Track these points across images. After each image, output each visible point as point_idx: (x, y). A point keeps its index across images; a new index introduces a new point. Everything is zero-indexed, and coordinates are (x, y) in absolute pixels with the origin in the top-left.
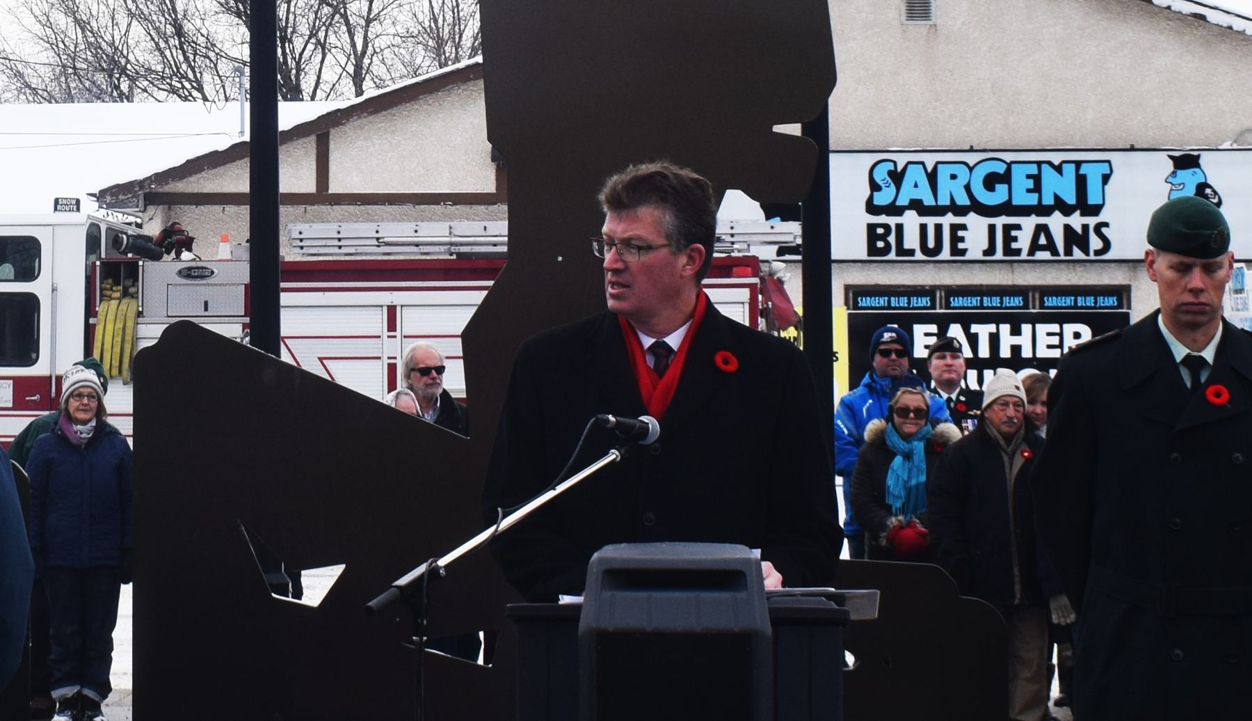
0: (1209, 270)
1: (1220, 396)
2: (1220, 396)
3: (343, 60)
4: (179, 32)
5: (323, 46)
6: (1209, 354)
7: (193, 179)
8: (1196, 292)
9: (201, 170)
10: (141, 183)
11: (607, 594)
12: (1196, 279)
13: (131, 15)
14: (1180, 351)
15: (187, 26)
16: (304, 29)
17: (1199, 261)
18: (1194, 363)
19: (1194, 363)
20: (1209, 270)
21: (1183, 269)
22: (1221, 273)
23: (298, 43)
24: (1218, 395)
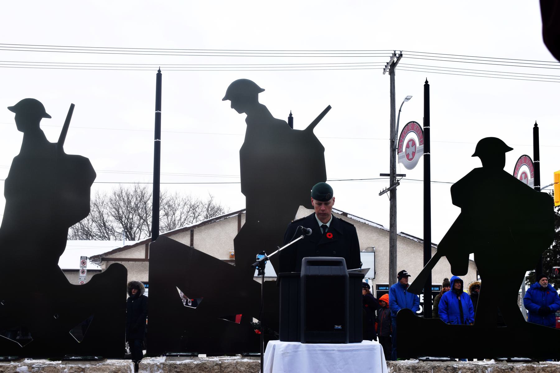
0: (326, 204)
1: (330, 236)
2: (330, 236)
3: (146, 232)
4: (104, 224)
5: (140, 230)
6: (328, 225)
7: (114, 255)
8: (323, 210)
9: (116, 252)
10: (101, 255)
11: (308, 267)
12: (323, 207)
13: (93, 221)
14: (321, 224)
15: (107, 224)
16: (136, 226)
17: (323, 203)
18: (324, 227)
19: (324, 227)
20: (326, 204)
21: (320, 204)
22: (330, 205)
23: (135, 229)
24: (330, 236)
